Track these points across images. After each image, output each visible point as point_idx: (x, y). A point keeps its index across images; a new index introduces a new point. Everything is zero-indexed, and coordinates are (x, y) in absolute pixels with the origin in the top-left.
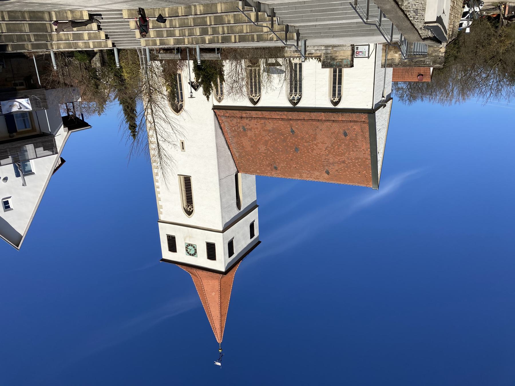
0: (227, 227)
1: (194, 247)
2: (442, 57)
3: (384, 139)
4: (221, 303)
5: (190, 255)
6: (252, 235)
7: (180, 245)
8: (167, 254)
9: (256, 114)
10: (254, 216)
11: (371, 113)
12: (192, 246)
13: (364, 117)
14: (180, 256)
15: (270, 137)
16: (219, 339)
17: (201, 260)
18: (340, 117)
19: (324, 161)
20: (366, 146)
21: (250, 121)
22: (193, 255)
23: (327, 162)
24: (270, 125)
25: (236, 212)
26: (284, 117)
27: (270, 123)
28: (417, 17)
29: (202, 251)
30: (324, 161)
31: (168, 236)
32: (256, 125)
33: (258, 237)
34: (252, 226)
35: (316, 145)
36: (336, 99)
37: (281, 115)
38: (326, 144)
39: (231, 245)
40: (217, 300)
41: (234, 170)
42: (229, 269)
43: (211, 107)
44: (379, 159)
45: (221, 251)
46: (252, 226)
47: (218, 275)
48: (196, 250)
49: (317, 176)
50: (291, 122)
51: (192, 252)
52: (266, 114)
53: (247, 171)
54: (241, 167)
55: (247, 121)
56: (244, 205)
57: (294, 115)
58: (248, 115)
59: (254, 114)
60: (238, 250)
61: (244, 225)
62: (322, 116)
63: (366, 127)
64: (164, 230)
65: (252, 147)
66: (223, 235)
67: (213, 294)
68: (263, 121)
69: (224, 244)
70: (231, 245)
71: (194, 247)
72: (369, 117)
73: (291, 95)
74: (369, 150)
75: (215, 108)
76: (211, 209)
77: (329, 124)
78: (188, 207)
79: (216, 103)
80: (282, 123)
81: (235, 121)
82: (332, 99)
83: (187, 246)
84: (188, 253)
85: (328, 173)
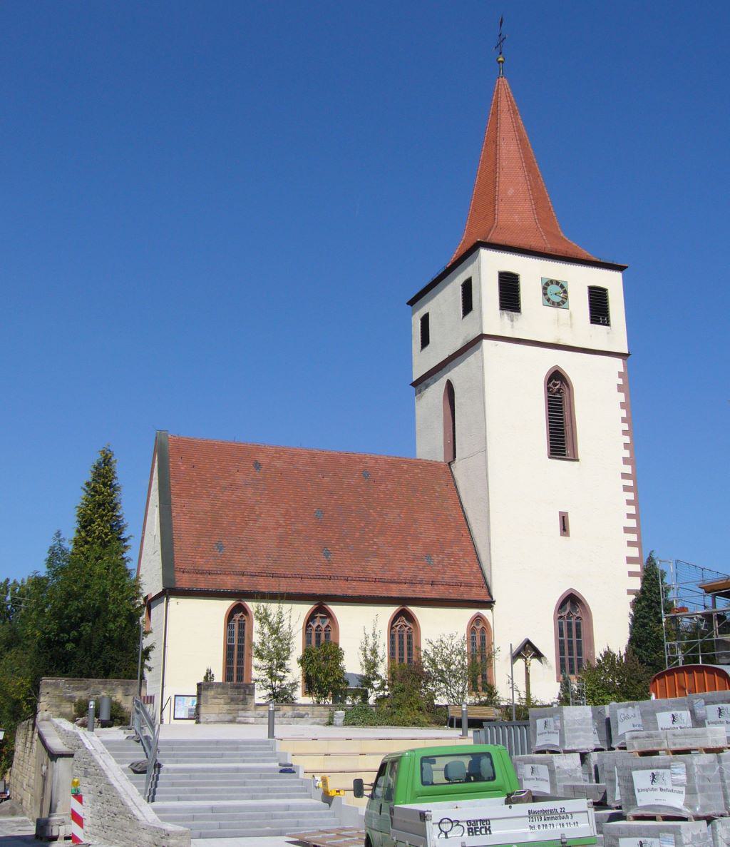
0: (474, 344)
1: (548, 300)
2: (44, 696)
3: (413, 808)
4: (494, 171)
5: (557, 283)
6: (425, 320)
7: (580, 303)
8: (612, 281)
9: (401, 591)
10: (422, 362)
11: (170, 591)
12: (553, 303)
13: (183, 581)
14: (580, 279)
15: (375, 543)
16: (503, 84)
17: (531, 272)
18: (229, 583)
19: (265, 489)
20: (179, 522)
21: (416, 577)
22: (552, 282)
23: (258, 489)
24: (374, 566)
25: (456, 374)
26: (342, 584)
27: (374, 572)
28: (86, 766)
29: (530, 293)
30: (265, 489)
31: (608, 321)
32: (403, 568)
33: (413, 314)
34: (425, 341)
35: (280, 525)
36: (237, 616)
37: (349, 588)
38: (259, 527)
39: (467, 307)
40: (502, 179)
41: (458, 470)
42: (469, 253)
43: (496, 607)
44: (157, 510)
45: (488, 293)
46: (425, 341)
47: (494, 241)
48: (545, 294)
49: (279, 458)
50: (328, 573)
51: (553, 289)
52: (380, 591)
53: (430, 466)
54: (445, 470)
55: (421, 575)
56: (436, 391)
57: (319, 588)
58: (418, 588)
59: (407, 592)
60: (451, 293)
61: (445, 341)
62: (263, 585)
63: (179, 562)
64: (616, 335)
65: (415, 521)
66: (481, 327)
67: (511, 192)
68: (388, 575)
69: (480, 307)
70: (467, 307)
71: (548, 300)
72: (173, 580)
73: (328, 626)
74: (173, 514)
75: (489, 604)
76: (507, 390)
77: (252, 569)
78: (559, 389)
79: (485, 613)
80: (347, 573)
81: (448, 576)
82: (245, 618)
83: (564, 303)
84: (562, 287)
85: (257, 466)
